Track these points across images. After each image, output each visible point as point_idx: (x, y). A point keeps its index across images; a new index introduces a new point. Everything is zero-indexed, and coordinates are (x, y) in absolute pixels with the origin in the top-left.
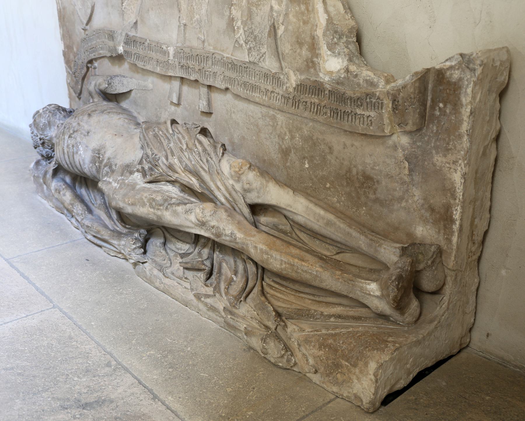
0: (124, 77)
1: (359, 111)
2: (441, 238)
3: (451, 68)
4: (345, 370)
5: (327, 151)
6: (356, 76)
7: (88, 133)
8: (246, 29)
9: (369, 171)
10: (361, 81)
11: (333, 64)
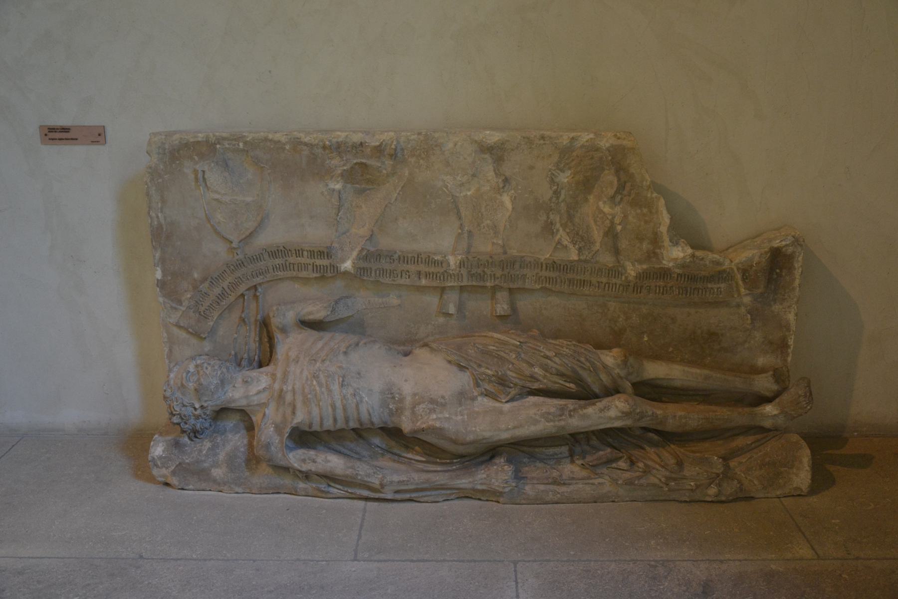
0: (347, 297)
1: (709, 286)
2: (779, 361)
3: (787, 245)
6: (703, 259)
7: (359, 374)
8: (568, 231)
10: (707, 263)
11: (676, 254)
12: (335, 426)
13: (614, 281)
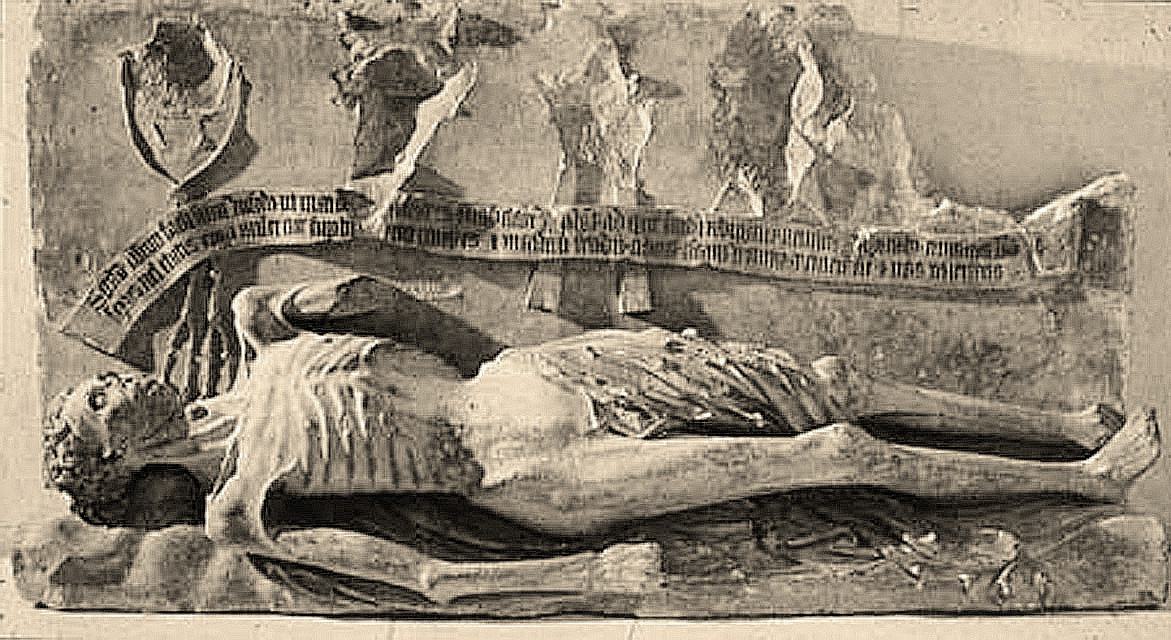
4: (1121, 567)
5: (917, 324)
9: (992, 339)
12: (350, 482)
13: (822, 254)
